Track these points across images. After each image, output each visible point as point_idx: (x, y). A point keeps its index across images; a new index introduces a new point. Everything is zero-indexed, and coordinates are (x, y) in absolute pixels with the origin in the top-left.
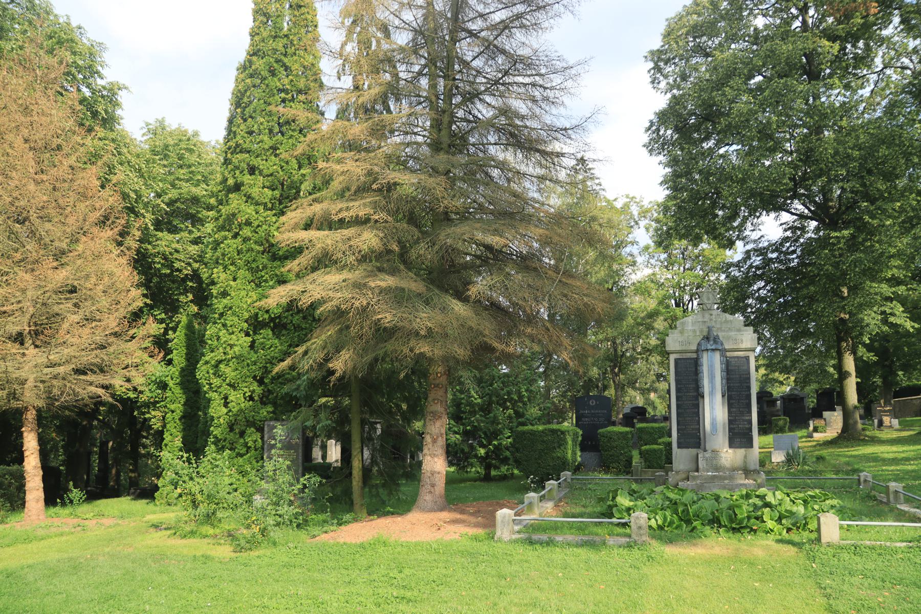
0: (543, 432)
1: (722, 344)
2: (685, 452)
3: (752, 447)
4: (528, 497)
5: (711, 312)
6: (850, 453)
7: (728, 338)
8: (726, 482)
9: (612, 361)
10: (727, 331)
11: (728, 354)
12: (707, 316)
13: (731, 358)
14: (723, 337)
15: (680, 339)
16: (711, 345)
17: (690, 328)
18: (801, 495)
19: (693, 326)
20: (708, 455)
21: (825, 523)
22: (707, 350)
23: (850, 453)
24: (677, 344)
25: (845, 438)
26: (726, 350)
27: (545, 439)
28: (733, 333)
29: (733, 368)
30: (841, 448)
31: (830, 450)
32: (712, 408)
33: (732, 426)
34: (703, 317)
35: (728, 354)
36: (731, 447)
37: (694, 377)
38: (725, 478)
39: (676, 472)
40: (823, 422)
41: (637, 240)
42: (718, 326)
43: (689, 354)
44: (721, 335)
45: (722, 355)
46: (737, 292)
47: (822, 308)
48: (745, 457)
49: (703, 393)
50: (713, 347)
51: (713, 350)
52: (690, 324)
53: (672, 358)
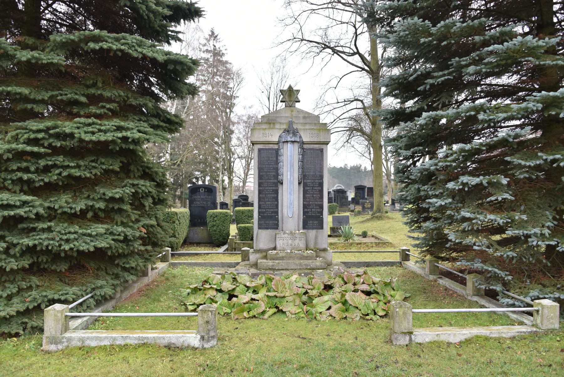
16: (291, 138)
22: (287, 142)
26: (303, 143)
33: (306, 210)
50: (293, 139)
51: (293, 142)
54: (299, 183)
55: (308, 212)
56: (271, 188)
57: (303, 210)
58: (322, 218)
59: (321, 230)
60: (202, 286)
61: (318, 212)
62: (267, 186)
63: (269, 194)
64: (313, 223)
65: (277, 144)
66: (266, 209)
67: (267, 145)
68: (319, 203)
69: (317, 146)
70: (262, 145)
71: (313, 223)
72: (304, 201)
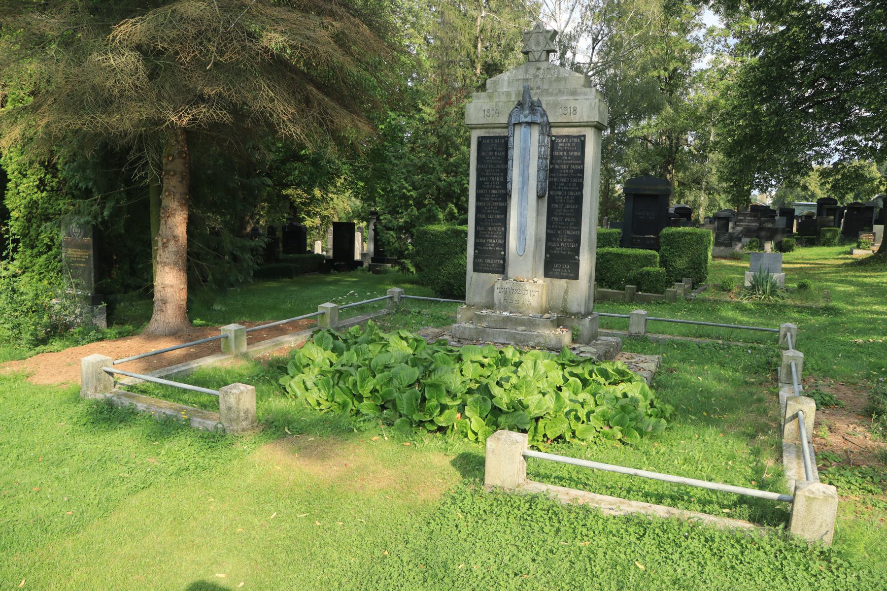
0: (445, 233)
1: (544, 114)
4: (224, 329)
5: (539, 64)
6: (860, 279)
7: (555, 105)
8: (520, 328)
9: (664, 156)
10: (556, 94)
11: (554, 131)
12: (532, 70)
13: (557, 137)
14: (547, 104)
15: (486, 107)
16: (526, 117)
17: (505, 89)
19: (509, 86)
20: (507, 284)
21: (493, 451)
22: (520, 124)
23: (860, 279)
24: (481, 114)
25: (880, 258)
26: (550, 125)
27: (447, 241)
28: (565, 98)
29: (559, 154)
30: (866, 271)
31: (852, 273)
32: (521, 215)
33: (550, 244)
34: (526, 72)
35: (554, 131)
36: (546, 275)
37: (502, 166)
38: (521, 323)
39: (469, 306)
40: (871, 236)
41: (704, 22)
42: (546, 86)
43: (499, 130)
44: (545, 100)
45: (542, 133)
46: (762, 72)
47: (863, 93)
48: (566, 292)
49: (510, 191)
50: (528, 119)
51: (530, 124)
52: (506, 83)
54: (540, 197)
55: (553, 248)
56: (496, 204)
58: (466, 241)
59: (573, 281)
61: (572, 250)
62: (490, 201)
63: (492, 213)
64: (561, 268)
65: (507, 128)
67: (491, 130)
68: (573, 233)
70: (483, 130)
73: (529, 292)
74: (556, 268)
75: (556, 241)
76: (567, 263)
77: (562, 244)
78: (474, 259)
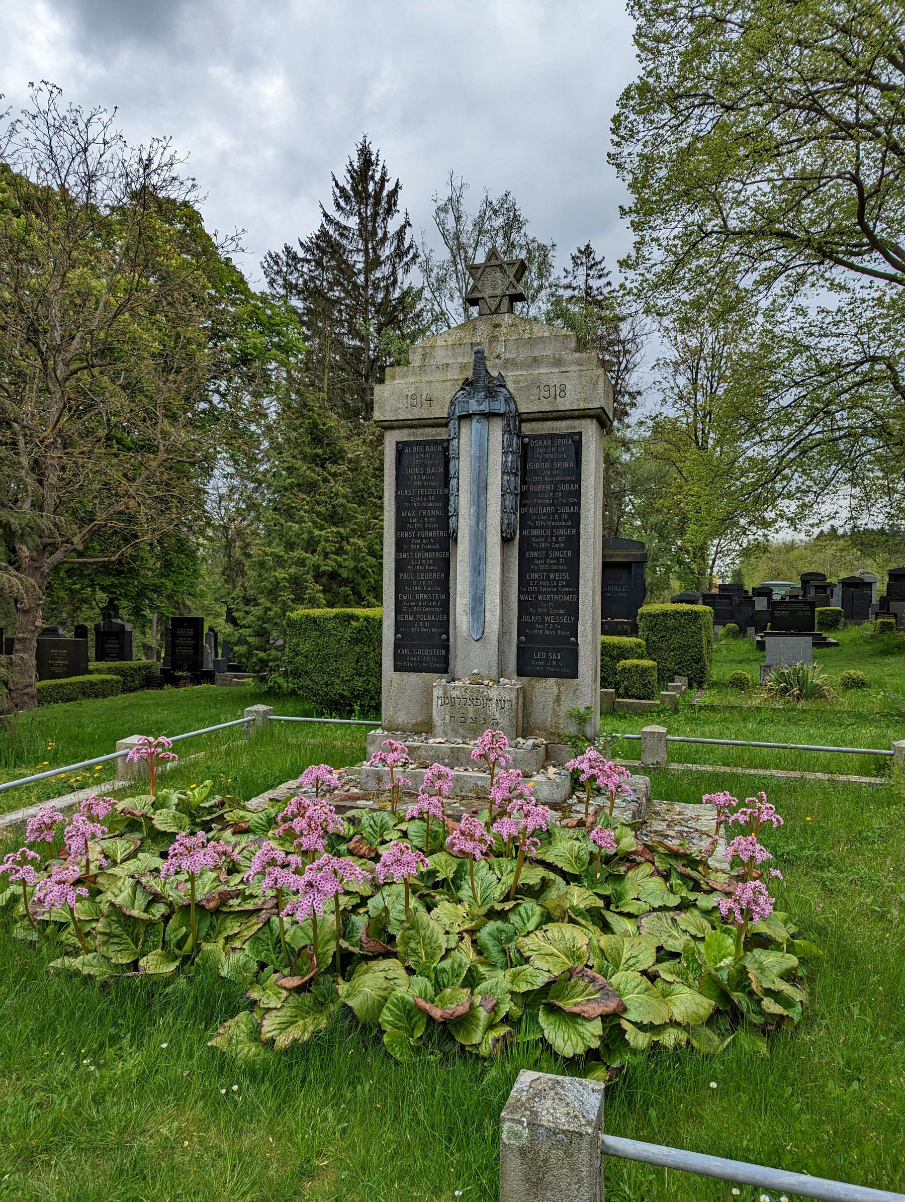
2: (413, 678)
3: (574, 674)
13: (534, 437)
18: (223, 959)
22: (468, 417)
26: (523, 418)
33: (526, 619)
37: (440, 491)
43: (433, 431)
50: (485, 407)
51: (488, 416)
53: (391, 439)
55: (532, 626)
57: (520, 618)
60: (146, 910)
61: (564, 627)
62: (420, 550)
64: (547, 660)
66: (414, 614)
67: (419, 431)
69: (562, 427)
70: (406, 431)
71: (547, 660)
72: (520, 592)
73: (494, 701)
74: (537, 660)
75: (536, 614)
76: (558, 650)
77: (547, 619)
78: (395, 648)
